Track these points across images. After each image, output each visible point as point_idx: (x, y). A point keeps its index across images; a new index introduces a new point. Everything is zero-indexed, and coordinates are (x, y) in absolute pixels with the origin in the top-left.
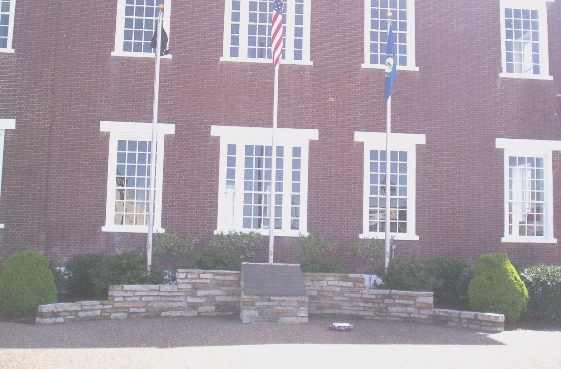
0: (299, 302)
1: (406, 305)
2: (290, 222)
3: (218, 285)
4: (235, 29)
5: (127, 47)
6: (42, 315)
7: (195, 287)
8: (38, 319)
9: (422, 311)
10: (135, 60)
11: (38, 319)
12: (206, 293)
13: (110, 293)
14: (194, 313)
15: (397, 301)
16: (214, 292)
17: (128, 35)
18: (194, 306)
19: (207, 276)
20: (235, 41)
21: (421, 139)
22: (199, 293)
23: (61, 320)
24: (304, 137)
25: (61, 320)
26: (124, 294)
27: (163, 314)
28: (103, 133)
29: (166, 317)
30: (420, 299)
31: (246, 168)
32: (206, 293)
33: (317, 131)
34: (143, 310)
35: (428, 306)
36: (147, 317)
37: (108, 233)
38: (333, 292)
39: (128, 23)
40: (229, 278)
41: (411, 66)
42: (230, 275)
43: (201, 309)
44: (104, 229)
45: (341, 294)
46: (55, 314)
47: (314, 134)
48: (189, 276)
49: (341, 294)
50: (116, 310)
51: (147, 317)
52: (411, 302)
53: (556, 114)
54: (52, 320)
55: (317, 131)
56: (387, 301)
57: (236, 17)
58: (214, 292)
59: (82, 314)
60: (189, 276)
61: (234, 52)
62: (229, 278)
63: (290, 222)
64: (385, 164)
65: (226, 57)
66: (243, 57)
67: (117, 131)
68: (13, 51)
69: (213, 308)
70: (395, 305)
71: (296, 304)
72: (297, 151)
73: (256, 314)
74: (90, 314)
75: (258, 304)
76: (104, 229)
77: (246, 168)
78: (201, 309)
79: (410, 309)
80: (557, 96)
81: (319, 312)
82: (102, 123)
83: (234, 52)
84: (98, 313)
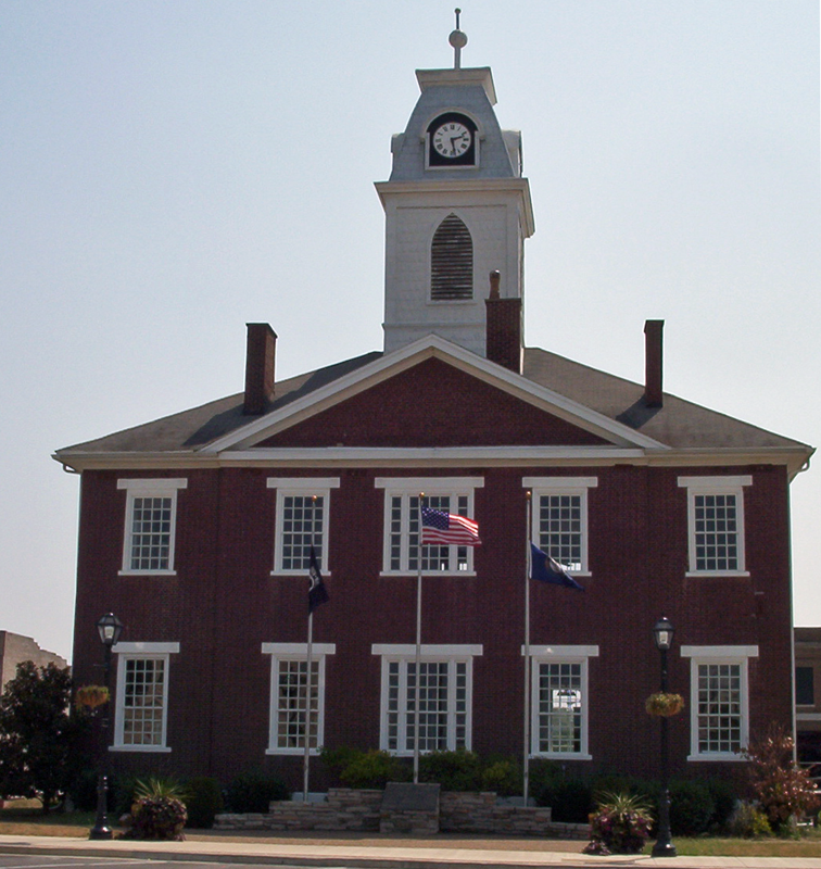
0: (428, 816)
1: (528, 819)
2: (459, 733)
3: (364, 803)
4: (396, 540)
5: (286, 565)
6: (218, 822)
7: (345, 805)
8: (215, 825)
9: (541, 825)
10: (294, 579)
11: (215, 825)
12: (354, 809)
13: (270, 808)
14: (344, 827)
15: (521, 816)
16: (361, 808)
17: (287, 552)
18: (343, 821)
19: (355, 795)
20: (396, 552)
21: (594, 651)
22: (348, 810)
23: (232, 827)
24: (470, 651)
25: (232, 827)
26: (282, 808)
27: (316, 827)
28: (265, 655)
29: (319, 830)
30: (538, 814)
31: (307, 762)
32: (354, 809)
33: (481, 646)
34: (298, 822)
35: (545, 820)
36: (301, 829)
37: (271, 756)
38: (468, 809)
39: (287, 539)
40: (373, 796)
41: (741, 572)
42: (375, 794)
43: (349, 824)
44: (267, 752)
45: (475, 811)
46: (228, 822)
47: (478, 650)
48: (339, 794)
49: (475, 811)
50: (276, 822)
51: (301, 829)
52: (531, 817)
53: (754, 615)
54: (226, 827)
55: (481, 646)
56: (513, 816)
57: (396, 527)
58: (361, 808)
59: (247, 823)
60: (339, 794)
61: (395, 565)
62: (373, 796)
63: (459, 733)
64: (420, 735)
65: (386, 571)
66: (404, 571)
67: (278, 652)
68: (174, 573)
69: (360, 823)
70: (519, 820)
71: (425, 817)
72: (461, 668)
73: (392, 825)
74: (255, 823)
75: (393, 817)
76: (267, 752)
77: (307, 762)
78: (349, 824)
79: (530, 823)
80: (756, 593)
81: (455, 827)
82: (263, 644)
83: (395, 565)
84: (261, 823)
